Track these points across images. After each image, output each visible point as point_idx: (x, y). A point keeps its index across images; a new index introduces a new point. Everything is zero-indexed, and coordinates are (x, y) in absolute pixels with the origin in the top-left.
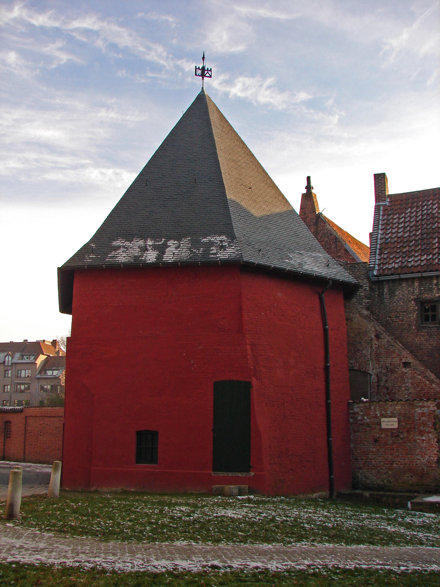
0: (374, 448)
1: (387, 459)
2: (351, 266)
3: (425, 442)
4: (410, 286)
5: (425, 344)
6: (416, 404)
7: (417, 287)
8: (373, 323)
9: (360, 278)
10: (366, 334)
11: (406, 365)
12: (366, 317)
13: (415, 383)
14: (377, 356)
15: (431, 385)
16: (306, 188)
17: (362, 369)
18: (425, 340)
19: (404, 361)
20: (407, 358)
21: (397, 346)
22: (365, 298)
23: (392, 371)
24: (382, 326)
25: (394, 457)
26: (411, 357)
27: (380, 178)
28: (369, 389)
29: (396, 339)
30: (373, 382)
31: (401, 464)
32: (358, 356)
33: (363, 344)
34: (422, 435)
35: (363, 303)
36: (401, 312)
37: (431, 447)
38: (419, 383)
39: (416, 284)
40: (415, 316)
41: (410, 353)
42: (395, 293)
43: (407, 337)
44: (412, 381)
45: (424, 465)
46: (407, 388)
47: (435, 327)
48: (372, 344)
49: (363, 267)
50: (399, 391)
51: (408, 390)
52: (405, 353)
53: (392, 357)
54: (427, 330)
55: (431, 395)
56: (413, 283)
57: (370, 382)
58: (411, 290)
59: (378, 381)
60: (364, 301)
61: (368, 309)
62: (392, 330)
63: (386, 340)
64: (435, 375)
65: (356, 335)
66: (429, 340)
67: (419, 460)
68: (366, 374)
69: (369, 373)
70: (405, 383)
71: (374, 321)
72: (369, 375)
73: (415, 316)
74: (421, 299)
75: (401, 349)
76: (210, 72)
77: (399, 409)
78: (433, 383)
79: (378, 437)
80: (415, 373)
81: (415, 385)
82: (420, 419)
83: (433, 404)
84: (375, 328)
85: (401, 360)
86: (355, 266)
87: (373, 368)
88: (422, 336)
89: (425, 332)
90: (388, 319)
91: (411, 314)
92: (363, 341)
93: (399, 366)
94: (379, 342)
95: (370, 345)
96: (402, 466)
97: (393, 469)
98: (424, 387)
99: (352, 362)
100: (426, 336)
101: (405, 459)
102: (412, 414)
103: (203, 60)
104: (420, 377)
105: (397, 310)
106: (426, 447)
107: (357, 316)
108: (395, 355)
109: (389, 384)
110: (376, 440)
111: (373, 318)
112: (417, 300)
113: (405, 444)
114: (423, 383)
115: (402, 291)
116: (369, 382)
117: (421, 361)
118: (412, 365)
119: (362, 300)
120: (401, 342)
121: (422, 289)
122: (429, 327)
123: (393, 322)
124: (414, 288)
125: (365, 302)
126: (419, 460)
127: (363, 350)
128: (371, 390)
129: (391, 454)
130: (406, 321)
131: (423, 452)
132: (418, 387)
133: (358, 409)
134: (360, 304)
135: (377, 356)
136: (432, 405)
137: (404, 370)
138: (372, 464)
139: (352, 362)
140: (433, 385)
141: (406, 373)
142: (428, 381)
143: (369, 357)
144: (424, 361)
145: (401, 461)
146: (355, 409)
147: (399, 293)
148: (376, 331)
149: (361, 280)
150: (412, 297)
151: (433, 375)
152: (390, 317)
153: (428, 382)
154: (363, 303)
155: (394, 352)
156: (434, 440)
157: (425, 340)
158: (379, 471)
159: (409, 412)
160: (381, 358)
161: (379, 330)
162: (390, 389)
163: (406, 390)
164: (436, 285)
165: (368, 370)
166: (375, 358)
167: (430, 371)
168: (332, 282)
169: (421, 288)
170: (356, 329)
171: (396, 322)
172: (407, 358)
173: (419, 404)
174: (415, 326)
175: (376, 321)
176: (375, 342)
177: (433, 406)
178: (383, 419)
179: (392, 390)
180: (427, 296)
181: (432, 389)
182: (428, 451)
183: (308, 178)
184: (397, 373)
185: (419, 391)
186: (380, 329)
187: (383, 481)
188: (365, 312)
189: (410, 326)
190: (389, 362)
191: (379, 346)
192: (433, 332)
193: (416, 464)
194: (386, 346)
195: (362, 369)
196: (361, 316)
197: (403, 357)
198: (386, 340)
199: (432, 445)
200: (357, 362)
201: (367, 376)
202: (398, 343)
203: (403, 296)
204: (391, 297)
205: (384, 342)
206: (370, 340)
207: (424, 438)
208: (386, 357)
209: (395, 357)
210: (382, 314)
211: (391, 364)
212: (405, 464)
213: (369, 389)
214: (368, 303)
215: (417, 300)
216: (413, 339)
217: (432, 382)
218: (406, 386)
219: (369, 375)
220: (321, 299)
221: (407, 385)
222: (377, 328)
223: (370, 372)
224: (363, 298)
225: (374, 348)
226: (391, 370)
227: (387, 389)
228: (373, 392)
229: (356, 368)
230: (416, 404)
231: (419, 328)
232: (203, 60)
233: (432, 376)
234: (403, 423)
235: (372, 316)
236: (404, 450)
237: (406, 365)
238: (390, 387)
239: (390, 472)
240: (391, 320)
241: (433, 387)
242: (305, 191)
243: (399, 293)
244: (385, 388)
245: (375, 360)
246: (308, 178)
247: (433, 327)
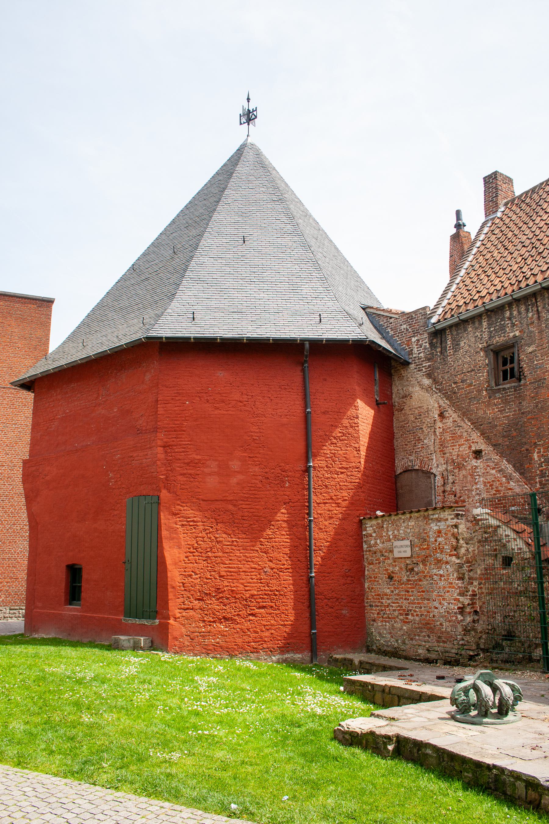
0: (388, 588)
1: (402, 607)
2: (408, 318)
3: (443, 579)
4: (476, 328)
5: (499, 418)
6: (432, 517)
7: (485, 329)
8: (436, 395)
9: (418, 332)
10: (428, 414)
11: (478, 454)
12: (428, 389)
13: (489, 482)
14: (441, 445)
15: (509, 483)
16: (455, 227)
17: (424, 468)
18: (499, 411)
19: (473, 449)
20: (477, 443)
21: (465, 426)
22: (425, 360)
23: (460, 467)
24: (447, 399)
25: (409, 603)
26: (482, 441)
27: (491, 181)
28: (433, 497)
29: (464, 416)
30: (438, 487)
31: (417, 615)
32: (419, 448)
33: (424, 429)
34: (440, 568)
35: (423, 369)
36: (468, 372)
37: (449, 587)
38: (493, 481)
39: (485, 324)
40: (485, 374)
41: (481, 435)
42: (459, 344)
43: (477, 410)
44: (485, 480)
45: (442, 617)
46: (478, 492)
47: (511, 388)
48: (435, 429)
49: (422, 316)
50: (469, 497)
51: (479, 494)
52: (475, 435)
53: (459, 445)
54: (502, 394)
55: (508, 499)
56: (481, 324)
57: (435, 486)
58: (479, 334)
59: (444, 483)
60: (424, 365)
61: (429, 376)
62: (458, 402)
63: (451, 419)
64: (514, 466)
65: (416, 419)
66: (505, 410)
67: (436, 608)
68: (429, 474)
69: (432, 473)
70: (476, 483)
71: (437, 393)
72: (432, 476)
73: (485, 374)
74: (491, 347)
75: (470, 430)
76: (255, 113)
77: (413, 526)
78: (511, 479)
79: (392, 572)
80: (488, 466)
81: (488, 485)
82: (436, 541)
83: (451, 515)
84: (438, 404)
85: (470, 447)
86: (412, 316)
87: (438, 465)
88: (496, 405)
89: (499, 398)
90: (453, 386)
91: (480, 373)
92: (425, 426)
93: (468, 457)
94: (443, 424)
95: (433, 430)
96: (417, 619)
97: (408, 622)
98: (500, 488)
99: (411, 458)
100: (500, 404)
101: (421, 608)
102: (426, 533)
103: (248, 102)
104: (494, 472)
105: (462, 370)
106: (445, 587)
107: (417, 388)
108: (462, 441)
109: (457, 488)
110: (391, 578)
111: (436, 388)
112: (486, 349)
113: (420, 583)
114: (499, 481)
115: (468, 340)
116: (433, 486)
117: (495, 445)
118: (483, 453)
119: (422, 364)
120: (469, 420)
121: (492, 329)
122: (504, 389)
123: (458, 389)
124: (482, 331)
125: (426, 366)
126: (436, 608)
127: (425, 439)
128: (435, 498)
129: (405, 599)
130: (474, 386)
131: (441, 596)
132: (492, 489)
133: (371, 529)
134: (419, 371)
135: (441, 445)
136: (450, 517)
137: (474, 462)
138: (386, 614)
139: (411, 458)
140: (511, 483)
141: (476, 467)
142: (504, 477)
143: (432, 448)
144: (500, 444)
145: (417, 610)
146: (368, 529)
147: (465, 343)
148: (440, 407)
149: (420, 335)
150: (480, 346)
151: (511, 466)
152: (455, 383)
153: (504, 479)
154: (423, 369)
155: (461, 437)
156: (453, 575)
157: (499, 411)
158: (393, 625)
159: (424, 530)
160: (447, 447)
161: (444, 405)
162: (458, 495)
163: (478, 494)
164: (510, 319)
165: (431, 468)
166: (440, 448)
167: (507, 460)
168: (310, 344)
169: (490, 328)
170: (416, 408)
171: (463, 388)
172: (477, 443)
173: (434, 517)
174: (486, 390)
175: (440, 392)
176: (439, 424)
177: (452, 519)
178: (397, 543)
179: (460, 497)
180: (499, 340)
181: (511, 489)
182: (447, 594)
183: (458, 213)
184: (466, 470)
185: (494, 494)
186: (445, 403)
187: (397, 641)
188: (427, 382)
189: (479, 391)
190: (456, 453)
191: (443, 430)
192: (508, 396)
193: (434, 616)
194: (451, 429)
195: (424, 468)
196: (423, 388)
197: (473, 442)
198: (451, 419)
199: (452, 583)
200: (417, 459)
201: (430, 478)
202: (466, 421)
203: (470, 346)
204: (455, 351)
205: (449, 422)
206: (433, 422)
207: (441, 572)
208: (451, 446)
209: (463, 444)
210: (445, 381)
211: (458, 455)
212: (421, 615)
213: (433, 497)
214: (429, 366)
215: (486, 349)
216: (485, 413)
217: (509, 478)
218: (477, 489)
219: (432, 476)
220: (303, 371)
221: (478, 486)
222: (441, 402)
223: (434, 471)
224: (423, 361)
225: (438, 434)
226: (458, 464)
227: (455, 496)
228: (438, 502)
229: (417, 467)
230: (432, 517)
231: (492, 392)
232: (248, 102)
233: (510, 469)
234: (417, 549)
235: (434, 386)
236: (419, 592)
237: (478, 454)
238: (458, 491)
239: (405, 628)
240: (457, 387)
241: (512, 487)
242: (454, 231)
243: (465, 343)
244: (452, 494)
245: (440, 451)
246: (458, 213)
247: (509, 388)
